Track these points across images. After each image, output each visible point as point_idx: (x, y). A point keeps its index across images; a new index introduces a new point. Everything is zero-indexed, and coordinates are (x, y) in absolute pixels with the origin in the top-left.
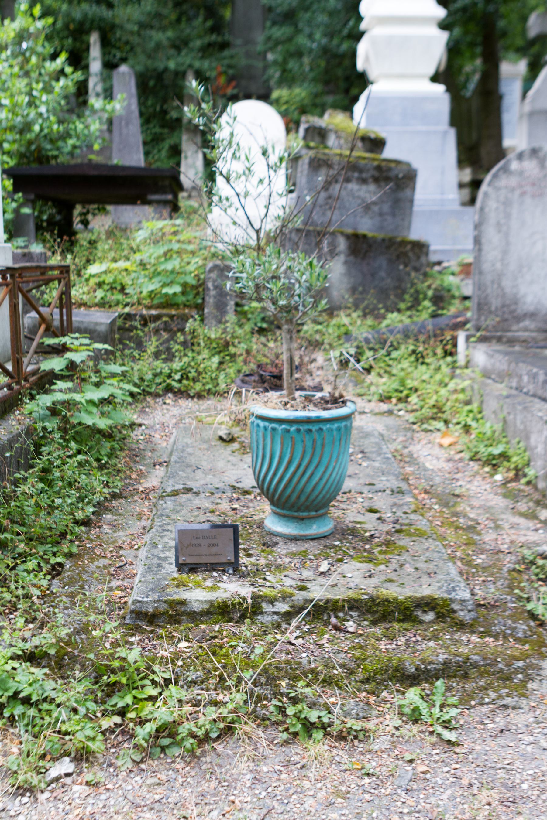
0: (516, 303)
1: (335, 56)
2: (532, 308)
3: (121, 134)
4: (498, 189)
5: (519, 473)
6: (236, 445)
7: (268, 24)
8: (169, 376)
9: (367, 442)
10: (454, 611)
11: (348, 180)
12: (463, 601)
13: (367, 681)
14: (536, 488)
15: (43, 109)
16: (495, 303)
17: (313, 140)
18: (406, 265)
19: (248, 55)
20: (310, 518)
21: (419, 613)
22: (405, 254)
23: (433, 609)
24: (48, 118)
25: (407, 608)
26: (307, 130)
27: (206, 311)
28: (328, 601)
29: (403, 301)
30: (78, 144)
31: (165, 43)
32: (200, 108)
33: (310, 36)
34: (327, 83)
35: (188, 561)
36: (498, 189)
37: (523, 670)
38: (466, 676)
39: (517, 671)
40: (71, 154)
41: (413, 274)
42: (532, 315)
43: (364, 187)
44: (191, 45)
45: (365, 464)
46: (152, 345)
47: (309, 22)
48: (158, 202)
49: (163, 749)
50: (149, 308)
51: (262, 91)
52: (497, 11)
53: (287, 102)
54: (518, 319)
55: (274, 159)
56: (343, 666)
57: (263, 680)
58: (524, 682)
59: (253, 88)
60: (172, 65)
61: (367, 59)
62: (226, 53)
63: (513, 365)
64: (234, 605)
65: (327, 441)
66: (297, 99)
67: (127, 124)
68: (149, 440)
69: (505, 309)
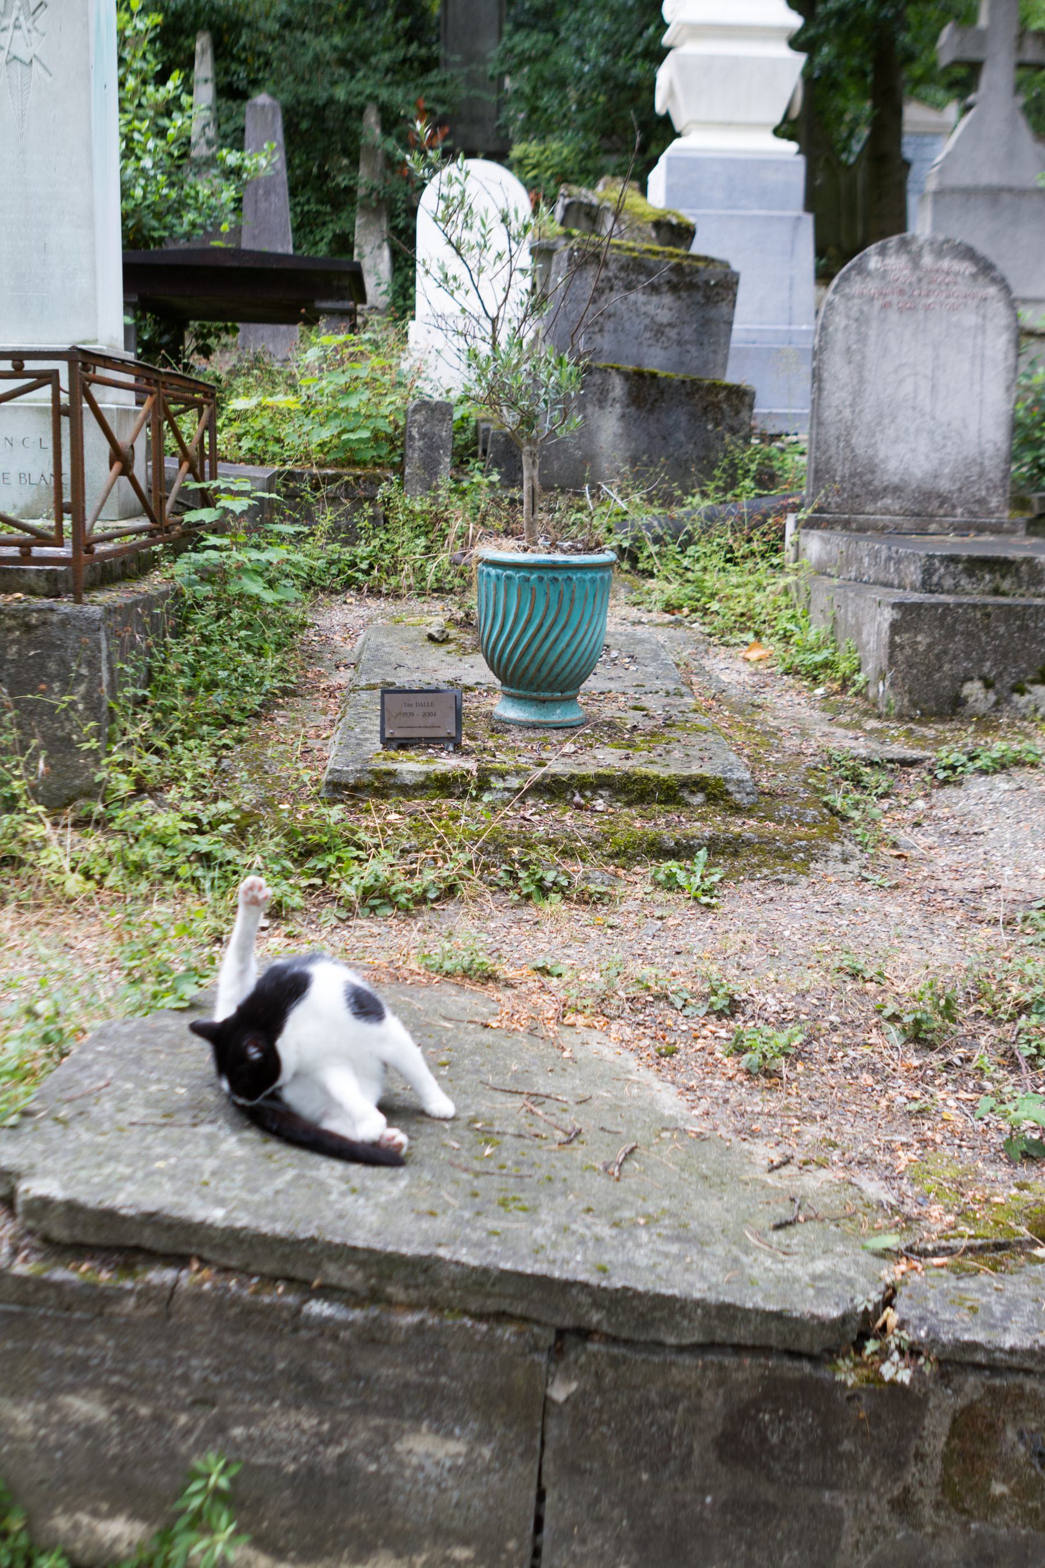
0: (873, 472)
1: (622, 87)
2: (896, 480)
3: (256, 211)
4: (849, 298)
5: (846, 683)
6: (452, 647)
7: (508, 27)
8: (353, 565)
9: (639, 648)
10: (728, 793)
11: (629, 287)
12: (740, 782)
13: (616, 855)
14: (866, 698)
15: (147, 162)
16: (841, 470)
17: (577, 226)
18: (717, 425)
19: (471, 81)
20: (553, 701)
21: (685, 794)
22: (717, 406)
23: (702, 790)
24: (155, 177)
25: (670, 788)
26: (567, 208)
27: (407, 471)
28: (573, 777)
29: (712, 478)
30: (199, 220)
31: (331, 56)
32: (426, 156)
33: (579, 52)
34: (606, 134)
35: (397, 735)
36: (849, 298)
37: (806, 850)
38: (736, 854)
39: (798, 850)
40: (188, 236)
41: (728, 437)
42: (896, 490)
43: (655, 299)
44: (373, 60)
45: (633, 668)
46: (326, 518)
47: (578, 28)
48: (331, 313)
49: (373, 909)
50: (321, 465)
51: (492, 147)
52: (899, 16)
53: (535, 167)
54: (876, 495)
55: (516, 227)
56: (588, 839)
57: (491, 848)
58: (805, 863)
59: (478, 141)
60: (340, 93)
61: (671, 94)
62: (434, 76)
63: (853, 545)
64: (455, 778)
65: (577, 595)
66: (556, 159)
67: (267, 193)
68: (327, 642)
69: (856, 480)
